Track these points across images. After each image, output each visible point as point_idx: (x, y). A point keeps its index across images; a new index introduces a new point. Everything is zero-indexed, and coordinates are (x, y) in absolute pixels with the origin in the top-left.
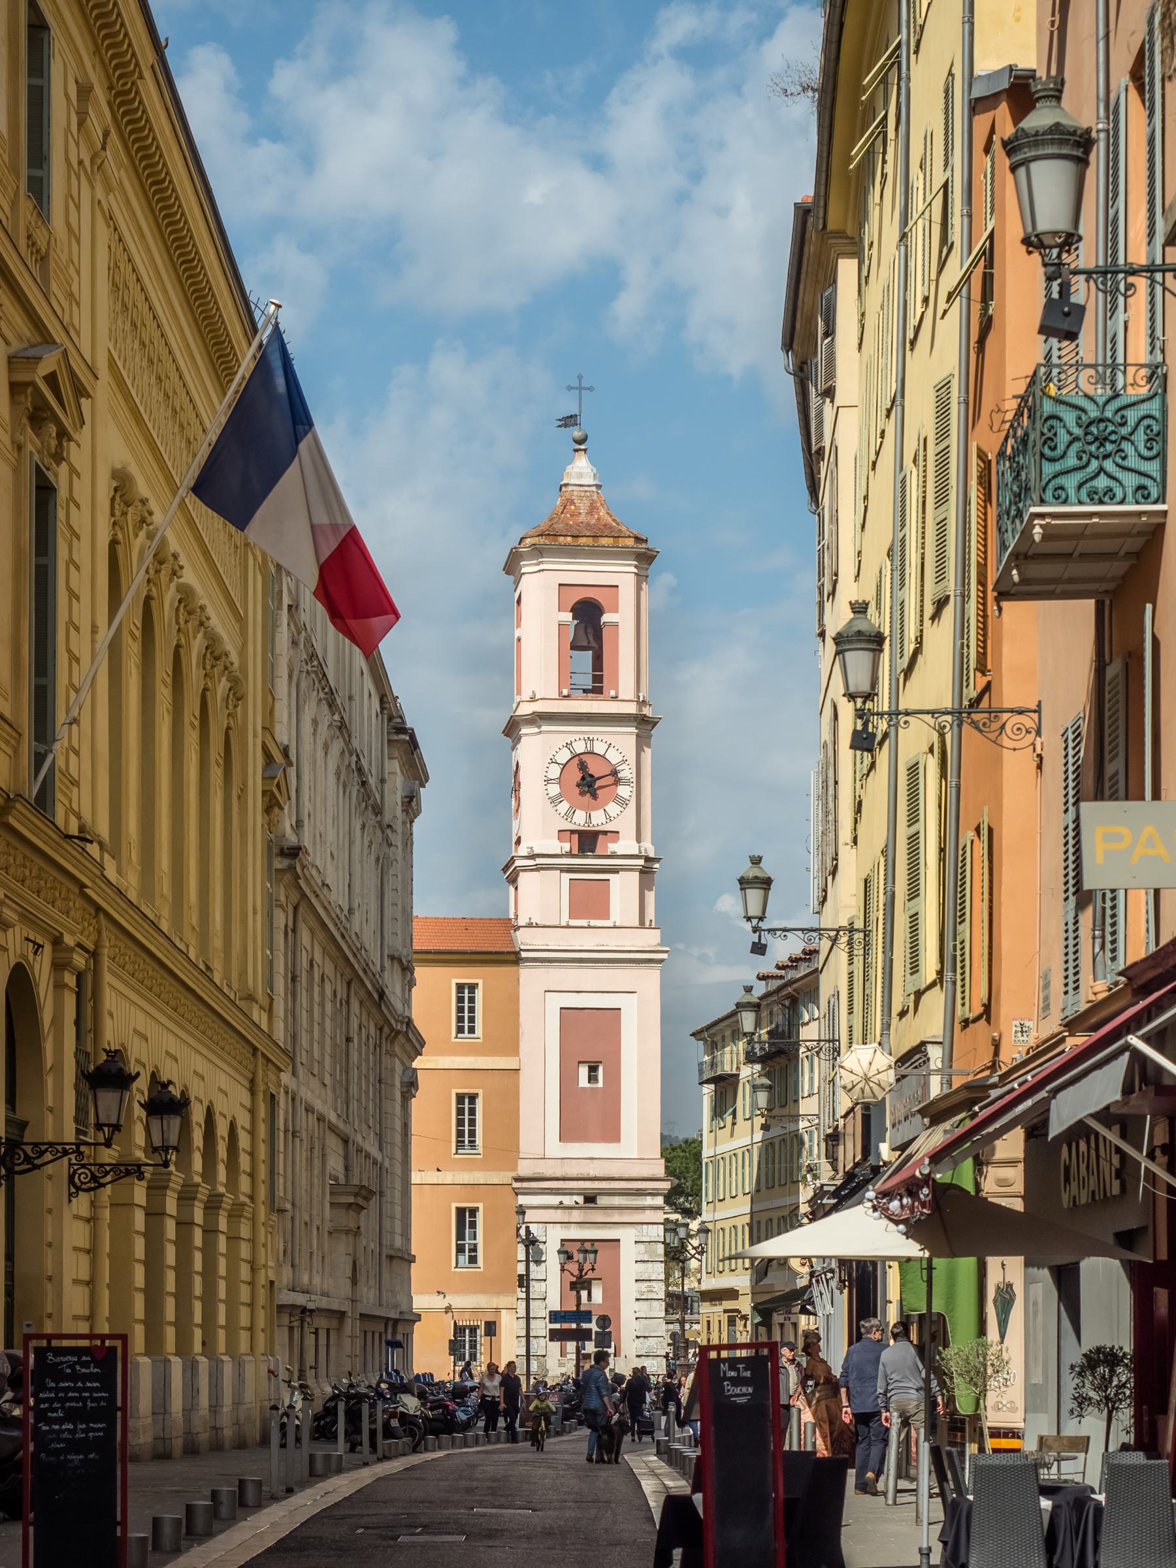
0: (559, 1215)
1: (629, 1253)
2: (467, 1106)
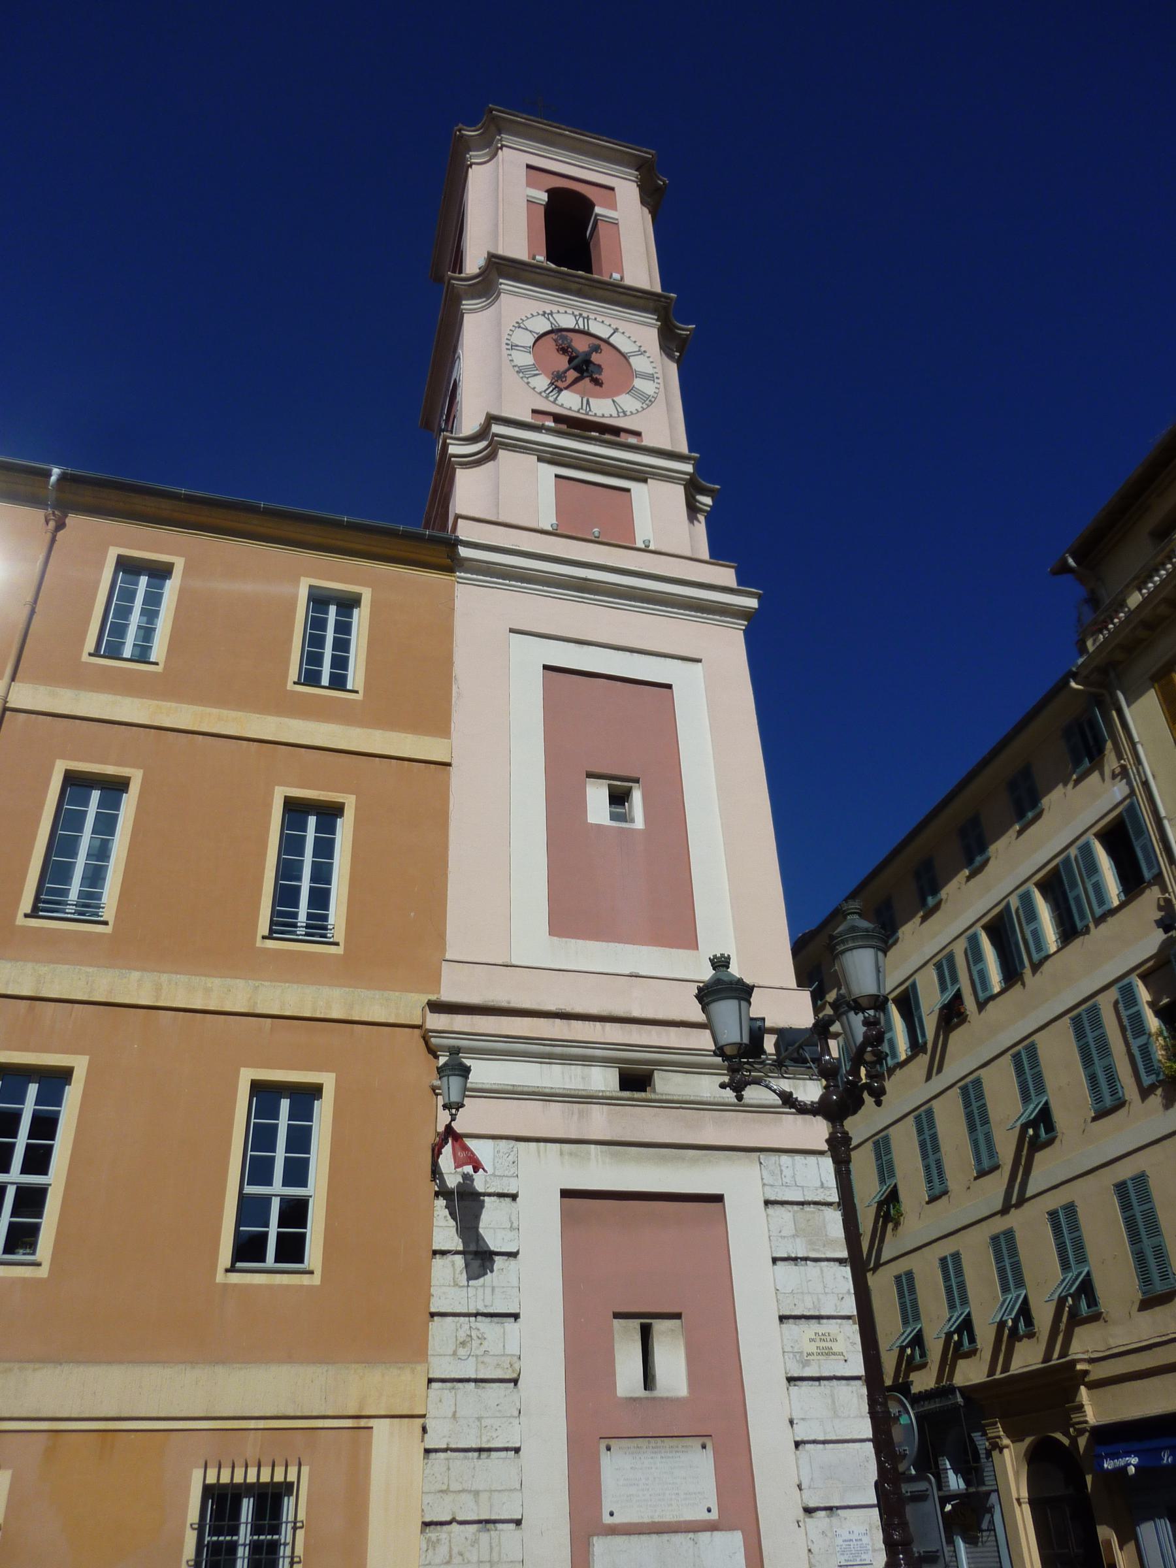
2: (283, 1123)
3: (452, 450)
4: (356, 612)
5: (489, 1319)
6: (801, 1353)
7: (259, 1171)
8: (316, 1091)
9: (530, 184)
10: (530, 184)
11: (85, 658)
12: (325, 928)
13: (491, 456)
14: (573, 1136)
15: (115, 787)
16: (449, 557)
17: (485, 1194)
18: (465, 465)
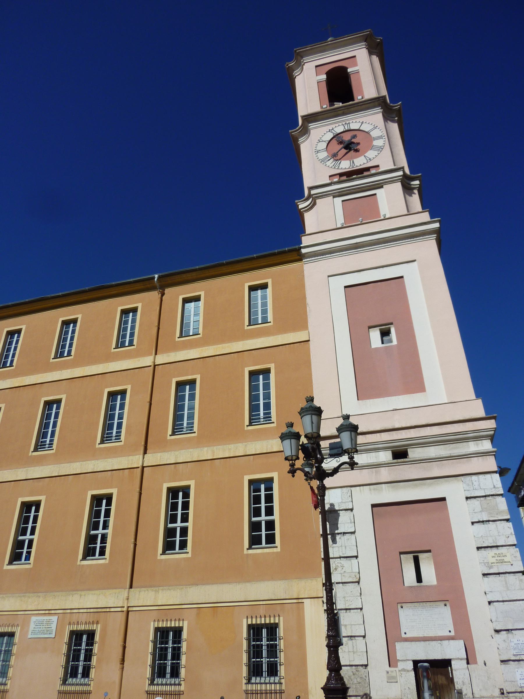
1: (460, 514)
3: (301, 207)
5: (345, 559)
6: (488, 563)
7: (257, 512)
11: (177, 339)
13: (315, 204)
15: (266, 372)
16: (298, 255)
17: (339, 510)
18: (307, 211)
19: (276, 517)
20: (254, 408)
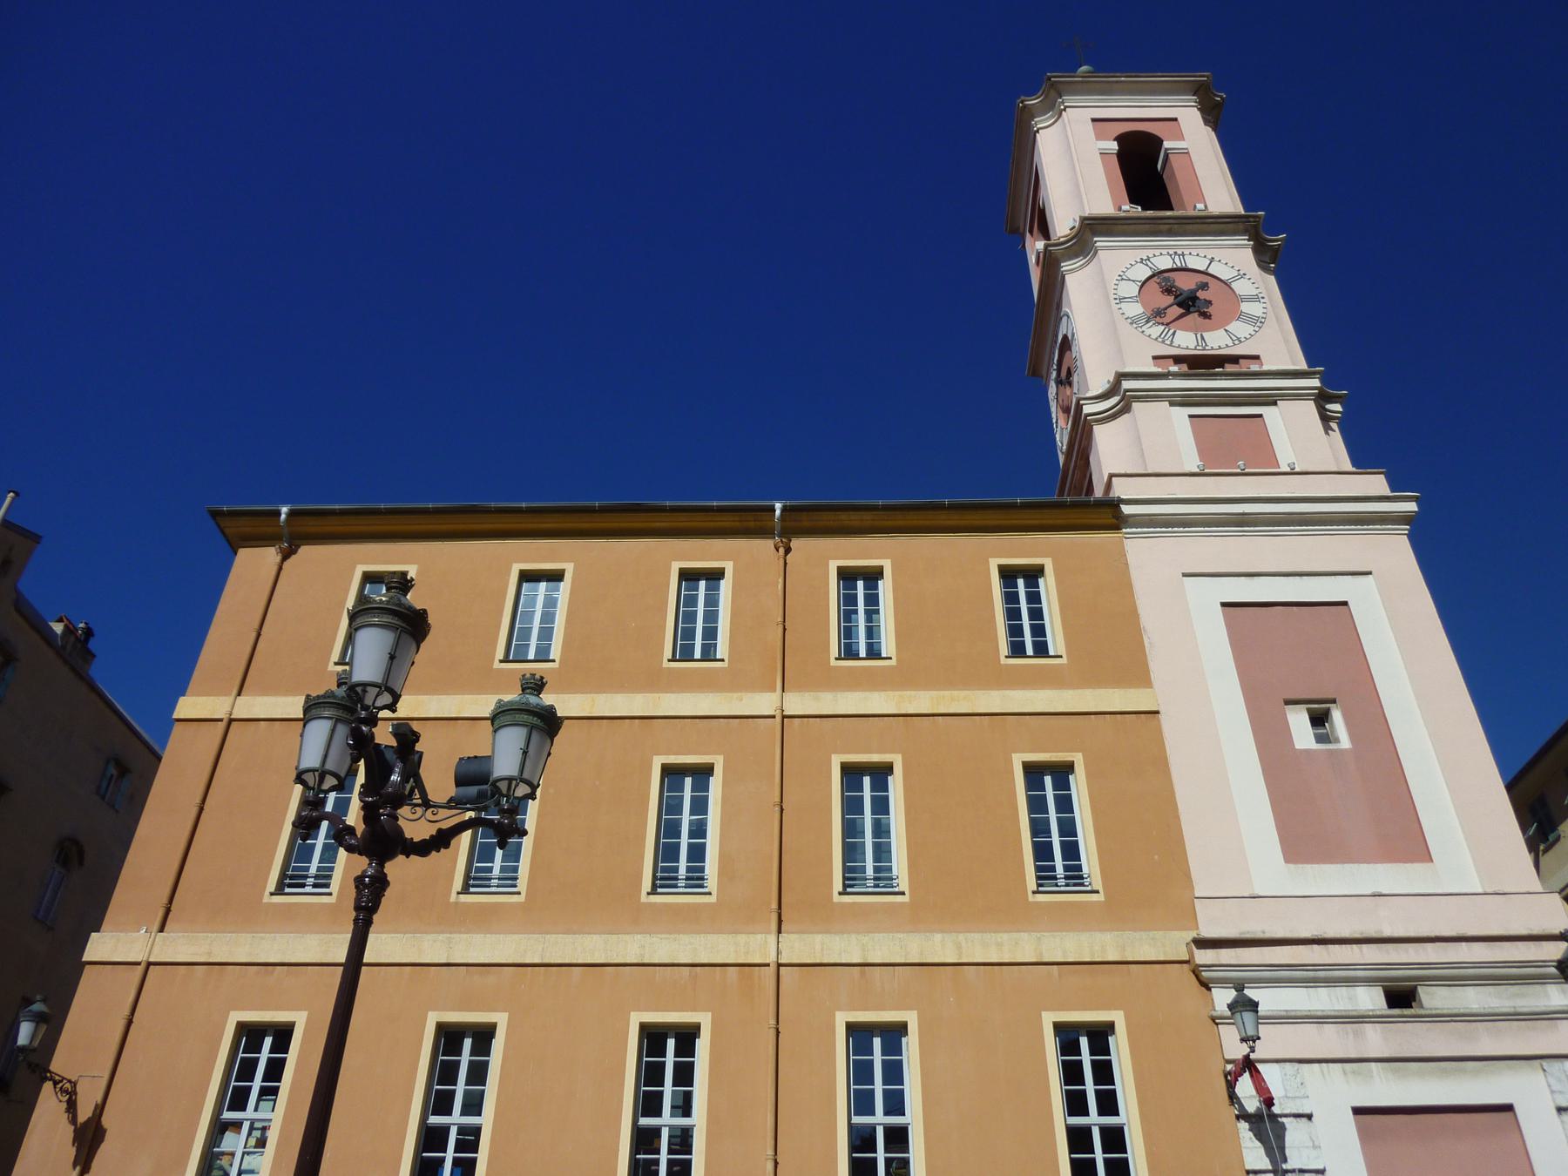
0: (1331, 1041)
2: (878, 1058)
3: (1087, 409)
4: (1041, 581)
7: (442, 1103)
8: (902, 1029)
9: (1099, 137)
10: (1099, 137)
12: (1081, 877)
13: (1126, 409)
14: (1353, 1055)
19: (486, 1120)
20: (667, 853)
